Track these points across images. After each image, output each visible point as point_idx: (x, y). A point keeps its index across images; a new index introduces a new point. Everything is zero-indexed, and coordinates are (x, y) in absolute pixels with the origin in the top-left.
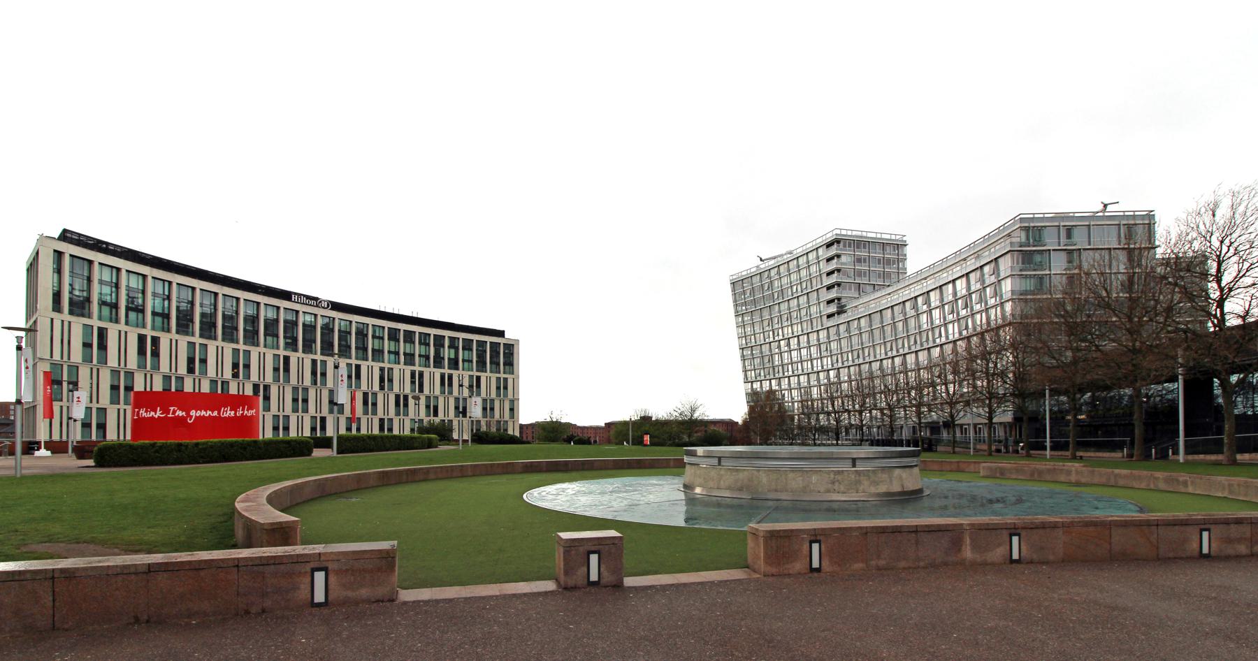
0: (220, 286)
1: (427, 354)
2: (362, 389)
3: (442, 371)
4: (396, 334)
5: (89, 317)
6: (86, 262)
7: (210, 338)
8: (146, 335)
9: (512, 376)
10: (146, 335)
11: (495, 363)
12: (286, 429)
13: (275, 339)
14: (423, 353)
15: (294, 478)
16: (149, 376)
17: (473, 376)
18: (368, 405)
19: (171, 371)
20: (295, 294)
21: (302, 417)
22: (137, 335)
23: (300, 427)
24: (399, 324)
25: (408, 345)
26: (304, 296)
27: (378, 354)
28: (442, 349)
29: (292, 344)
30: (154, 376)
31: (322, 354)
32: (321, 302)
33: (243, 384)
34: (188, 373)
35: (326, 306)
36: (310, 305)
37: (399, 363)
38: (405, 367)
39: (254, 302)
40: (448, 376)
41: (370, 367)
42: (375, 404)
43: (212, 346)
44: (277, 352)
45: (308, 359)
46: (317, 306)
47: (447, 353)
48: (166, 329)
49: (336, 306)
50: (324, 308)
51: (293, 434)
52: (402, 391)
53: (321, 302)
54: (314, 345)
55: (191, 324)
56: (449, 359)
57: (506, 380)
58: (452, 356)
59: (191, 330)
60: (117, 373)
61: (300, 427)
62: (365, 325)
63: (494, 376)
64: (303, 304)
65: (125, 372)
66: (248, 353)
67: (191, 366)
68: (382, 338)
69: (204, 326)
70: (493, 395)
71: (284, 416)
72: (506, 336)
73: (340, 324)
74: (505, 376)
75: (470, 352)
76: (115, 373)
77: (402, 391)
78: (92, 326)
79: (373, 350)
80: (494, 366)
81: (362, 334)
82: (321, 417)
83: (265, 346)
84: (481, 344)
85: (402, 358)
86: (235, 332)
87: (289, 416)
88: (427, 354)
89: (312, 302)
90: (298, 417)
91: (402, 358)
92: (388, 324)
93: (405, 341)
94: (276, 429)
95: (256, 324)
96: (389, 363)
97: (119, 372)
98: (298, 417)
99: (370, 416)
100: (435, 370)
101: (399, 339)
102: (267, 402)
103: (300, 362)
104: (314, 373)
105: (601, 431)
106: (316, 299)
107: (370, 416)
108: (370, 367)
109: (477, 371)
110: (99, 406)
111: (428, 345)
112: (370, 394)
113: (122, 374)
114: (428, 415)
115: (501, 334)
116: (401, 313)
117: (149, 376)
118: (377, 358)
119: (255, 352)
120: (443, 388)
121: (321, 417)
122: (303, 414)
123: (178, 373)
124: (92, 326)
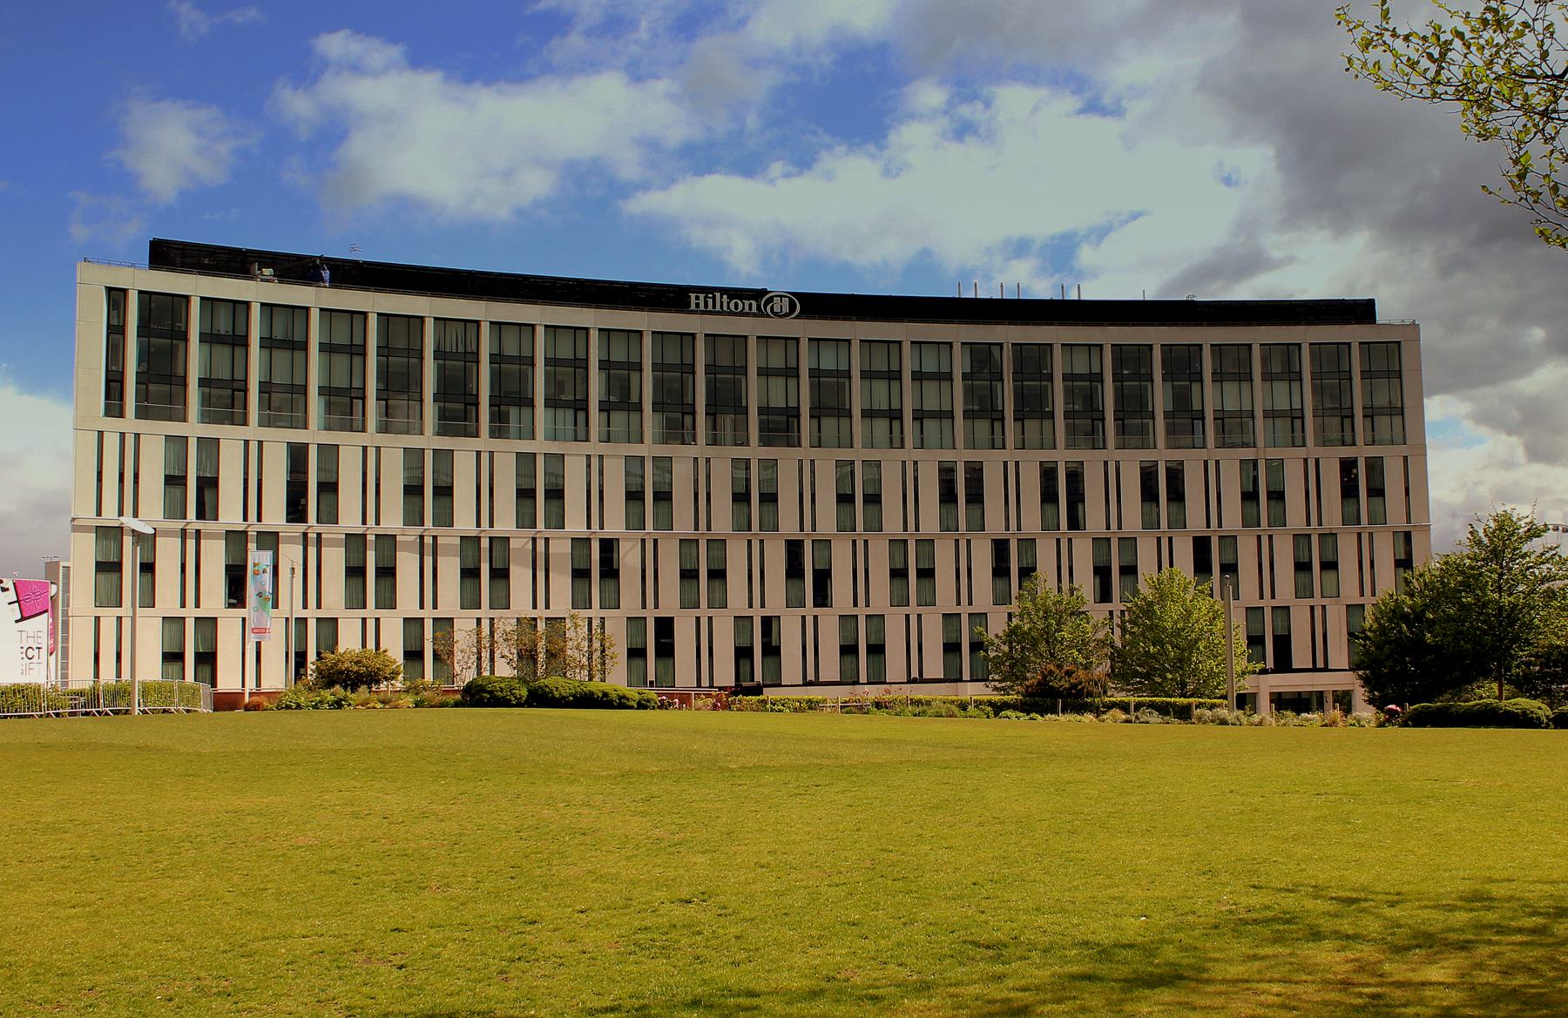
0: (482, 304)
9: (1402, 450)
11: (1032, 406)
12: (207, 659)
16: (963, 544)
17: (1255, 463)
18: (802, 577)
21: (919, 616)
26: (724, 291)
27: (1233, 428)
28: (1196, 387)
29: (457, 418)
32: (771, 300)
33: (969, 542)
34: (197, 518)
35: (786, 309)
38: (604, 449)
40: (1168, 470)
44: (845, 454)
45: (277, 443)
47: (1210, 396)
49: (815, 305)
55: (474, 408)
57: (1375, 466)
60: (828, 543)
63: (277, 443)
65: (1019, 540)
66: (210, 447)
72: (1380, 319)
74: (1373, 451)
79: (266, 388)
80: (982, 426)
84: (400, 329)
85: (315, 403)
87: (215, 620)
90: (698, 619)
91: (315, 403)
93: (1219, 377)
97: (1309, 535)
98: (698, 619)
99: (371, 611)
100: (268, 434)
102: (388, 581)
106: (758, 294)
108: (253, 448)
110: (1275, 603)
113: (1315, 540)
114: (1002, 598)
115: (1362, 311)
116: (981, 295)
117: (963, 544)
118: (399, 420)
119: (350, 447)
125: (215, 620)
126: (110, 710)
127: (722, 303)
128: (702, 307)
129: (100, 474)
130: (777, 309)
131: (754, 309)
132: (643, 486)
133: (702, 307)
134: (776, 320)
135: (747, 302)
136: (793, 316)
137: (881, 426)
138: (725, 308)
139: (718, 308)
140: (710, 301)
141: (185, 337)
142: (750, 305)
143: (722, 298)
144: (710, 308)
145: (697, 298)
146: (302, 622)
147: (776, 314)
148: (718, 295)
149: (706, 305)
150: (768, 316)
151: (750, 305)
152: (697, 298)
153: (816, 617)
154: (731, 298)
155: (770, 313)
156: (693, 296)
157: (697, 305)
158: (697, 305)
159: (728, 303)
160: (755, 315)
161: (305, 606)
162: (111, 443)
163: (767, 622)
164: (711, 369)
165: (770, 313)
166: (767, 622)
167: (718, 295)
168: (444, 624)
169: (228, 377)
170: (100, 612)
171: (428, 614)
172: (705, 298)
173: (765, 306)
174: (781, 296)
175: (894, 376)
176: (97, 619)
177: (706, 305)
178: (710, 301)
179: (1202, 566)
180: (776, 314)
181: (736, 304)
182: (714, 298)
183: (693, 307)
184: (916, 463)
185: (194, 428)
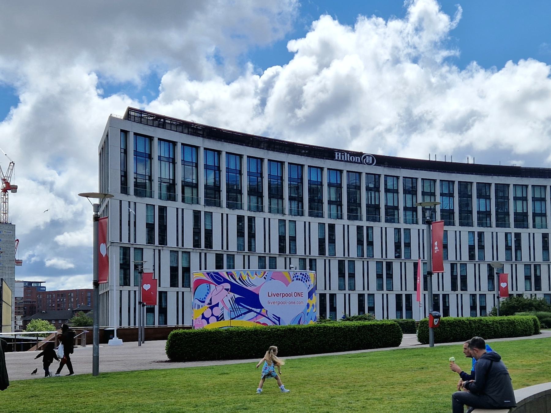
1: (488, 210)
2: (449, 259)
3: (507, 230)
4: (466, 188)
5: (151, 197)
6: (147, 139)
7: (374, 220)
8: (244, 216)
10: (244, 216)
13: (280, 201)
14: (409, 205)
15: (308, 358)
16: (246, 258)
19: (178, 245)
20: (339, 151)
22: (192, 212)
23: (460, 307)
24: (453, 175)
25: (482, 201)
30: (250, 257)
31: (516, 226)
32: (365, 157)
35: (371, 162)
36: (355, 162)
37: (417, 223)
39: (277, 162)
41: (495, 234)
42: (352, 276)
43: (377, 227)
45: (233, 215)
46: (361, 163)
47: (476, 205)
48: (488, 225)
49: (381, 161)
50: (368, 164)
51: (453, 316)
52: (132, 241)
53: (365, 157)
54: (396, 213)
56: (206, 187)
58: (211, 181)
59: (396, 217)
61: (460, 307)
62: (451, 184)
64: (347, 161)
66: (407, 231)
67: (472, 253)
68: (397, 191)
69: (208, 191)
70: (354, 253)
71: (368, 294)
73: (423, 186)
75: (488, 201)
76: (174, 253)
77: (132, 241)
78: (154, 206)
81: (465, 195)
82: (406, 295)
83: (270, 212)
84: (464, 186)
86: (434, 213)
87: (374, 294)
88: (488, 210)
89: (356, 159)
92: (438, 176)
94: (473, 308)
95: (300, 191)
96: (406, 222)
99: (459, 292)
100: (388, 225)
101: (490, 196)
103: (346, 229)
104: (360, 242)
105: (89, 294)
106: (360, 154)
107: (385, 292)
108: (495, 234)
109: (516, 226)
111: (488, 198)
112: (132, 251)
117: (246, 258)
120: (241, 239)
121: (406, 295)
122: (351, 292)
123: (388, 258)
124: (154, 206)
125: (374, 294)
126: (49, 341)
127: (347, 157)
128: (340, 159)
129: (121, 221)
130: (367, 162)
131: (359, 161)
132: (474, 243)
133: (340, 159)
134: (366, 166)
135: (356, 158)
136: (374, 164)
137: (409, 213)
138: (349, 160)
139: (346, 159)
140: (343, 156)
141: (471, 196)
142: (358, 159)
143: (347, 155)
144: (343, 159)
145: (338, 154)
146: (363, 295)
147: (367, 163)
148: (346, 154)
149: (341, 158)
150: (364, 164)
151: (358, 159)
152: (338, 154)
153: (349, 295)
154: (350, 156)
155: (365, 162)
156: (336, 153)
157: (338, 157)
158: (338, 157)
159: (350, 157)
160: (359, 163)
161: (512, 290)
162: (125, 205)
163: (444, 296)
164: (228, 170)
165: (365, 162)
166: (444, 296)
167: (346, 154)
168: (483, 296)
169: (449, 209)
170: (122, 288)
171: (478, 293)
172: (341, 154)
173: (364, 159)
174: (369, 156)
175: (433, 194)
176: (121, 291)
177: (341, 158)
178: (343, 156)
179: (262, 266)
180: (367, 163)
181: (353, 158)
182: (344, 155)
183: (337, 158)
184: (460, 232)
185: (476, 229)
